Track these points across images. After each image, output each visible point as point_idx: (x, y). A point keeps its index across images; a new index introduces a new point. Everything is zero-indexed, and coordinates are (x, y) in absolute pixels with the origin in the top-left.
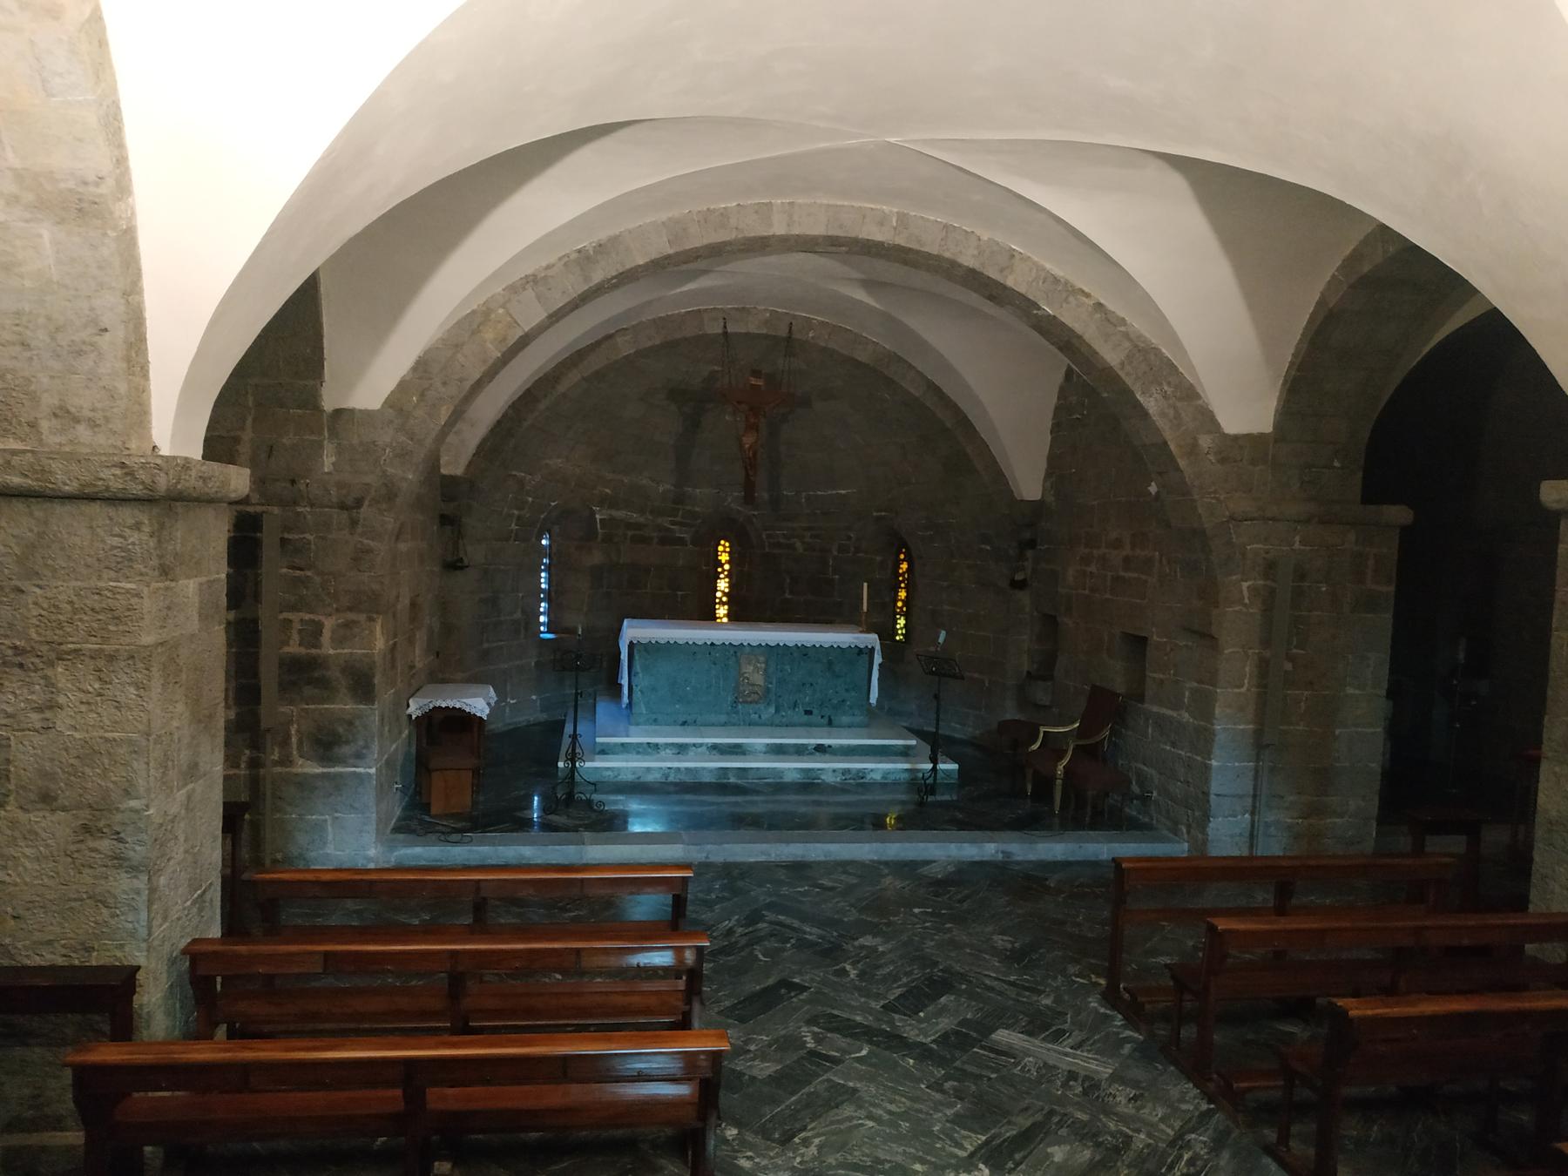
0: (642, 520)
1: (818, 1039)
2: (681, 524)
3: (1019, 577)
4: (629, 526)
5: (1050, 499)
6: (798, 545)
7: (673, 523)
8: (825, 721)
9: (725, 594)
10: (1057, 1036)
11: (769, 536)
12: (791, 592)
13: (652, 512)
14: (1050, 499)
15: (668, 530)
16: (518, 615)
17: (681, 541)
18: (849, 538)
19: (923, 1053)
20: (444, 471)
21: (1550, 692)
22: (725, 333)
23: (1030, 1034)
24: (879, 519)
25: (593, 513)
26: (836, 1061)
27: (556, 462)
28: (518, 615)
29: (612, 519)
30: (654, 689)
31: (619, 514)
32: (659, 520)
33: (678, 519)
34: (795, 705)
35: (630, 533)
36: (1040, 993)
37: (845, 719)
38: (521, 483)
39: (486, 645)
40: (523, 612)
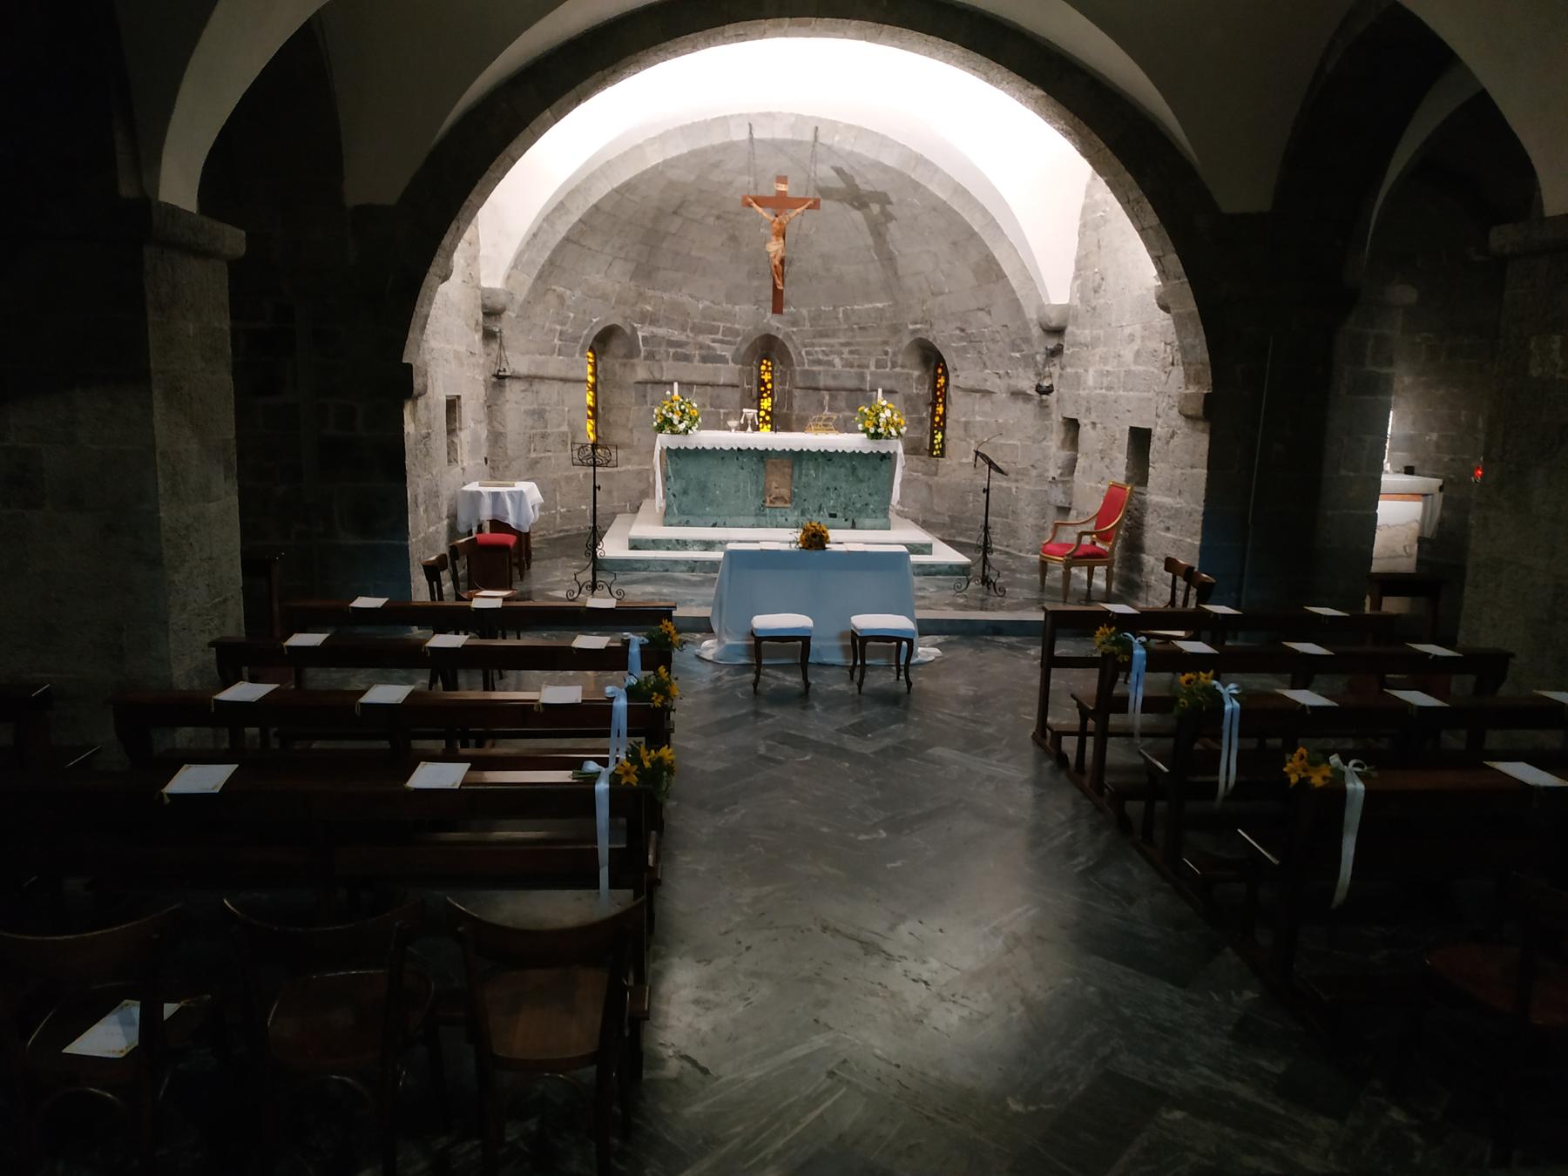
0: (683, 338)
1: (769, 748)
2: (722, 342)
3: (1046, 383)
4: (671, 343)
5: (1077, 302)
6: (837, 361)
7: (714, 341)
8: (849, 523)
9: (767, 413)
10: (987, 754)
11: (808, 353)
12: (830, 409)
13: (692, 329)
14: (1077, 302)
15: (709, 347)
16: (565, 428)
17: (722, 360)
18: (886, 353)
19: (860, 759)
20: (484, 284)
21: (1129, 177)
22: (751, 139)
23: (964, 751)
24: (914, 331)
25: (634, 330)
26: (779, 762)
27: (596, 278)
28: (565, 428)
29: (654, 336)
30: (685, 492)
31: (661, 331)
32: (701, 338)
33: (719, 336)
34: (820, 508)
35: (672, 351)
36: (986, 724)
37: (868, 522)
38: (561, 297)
39: (533, 455)
40: (569, 425)
